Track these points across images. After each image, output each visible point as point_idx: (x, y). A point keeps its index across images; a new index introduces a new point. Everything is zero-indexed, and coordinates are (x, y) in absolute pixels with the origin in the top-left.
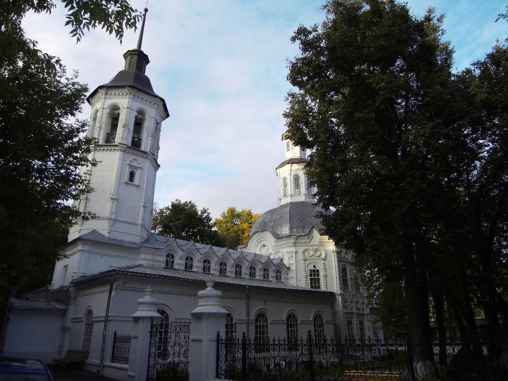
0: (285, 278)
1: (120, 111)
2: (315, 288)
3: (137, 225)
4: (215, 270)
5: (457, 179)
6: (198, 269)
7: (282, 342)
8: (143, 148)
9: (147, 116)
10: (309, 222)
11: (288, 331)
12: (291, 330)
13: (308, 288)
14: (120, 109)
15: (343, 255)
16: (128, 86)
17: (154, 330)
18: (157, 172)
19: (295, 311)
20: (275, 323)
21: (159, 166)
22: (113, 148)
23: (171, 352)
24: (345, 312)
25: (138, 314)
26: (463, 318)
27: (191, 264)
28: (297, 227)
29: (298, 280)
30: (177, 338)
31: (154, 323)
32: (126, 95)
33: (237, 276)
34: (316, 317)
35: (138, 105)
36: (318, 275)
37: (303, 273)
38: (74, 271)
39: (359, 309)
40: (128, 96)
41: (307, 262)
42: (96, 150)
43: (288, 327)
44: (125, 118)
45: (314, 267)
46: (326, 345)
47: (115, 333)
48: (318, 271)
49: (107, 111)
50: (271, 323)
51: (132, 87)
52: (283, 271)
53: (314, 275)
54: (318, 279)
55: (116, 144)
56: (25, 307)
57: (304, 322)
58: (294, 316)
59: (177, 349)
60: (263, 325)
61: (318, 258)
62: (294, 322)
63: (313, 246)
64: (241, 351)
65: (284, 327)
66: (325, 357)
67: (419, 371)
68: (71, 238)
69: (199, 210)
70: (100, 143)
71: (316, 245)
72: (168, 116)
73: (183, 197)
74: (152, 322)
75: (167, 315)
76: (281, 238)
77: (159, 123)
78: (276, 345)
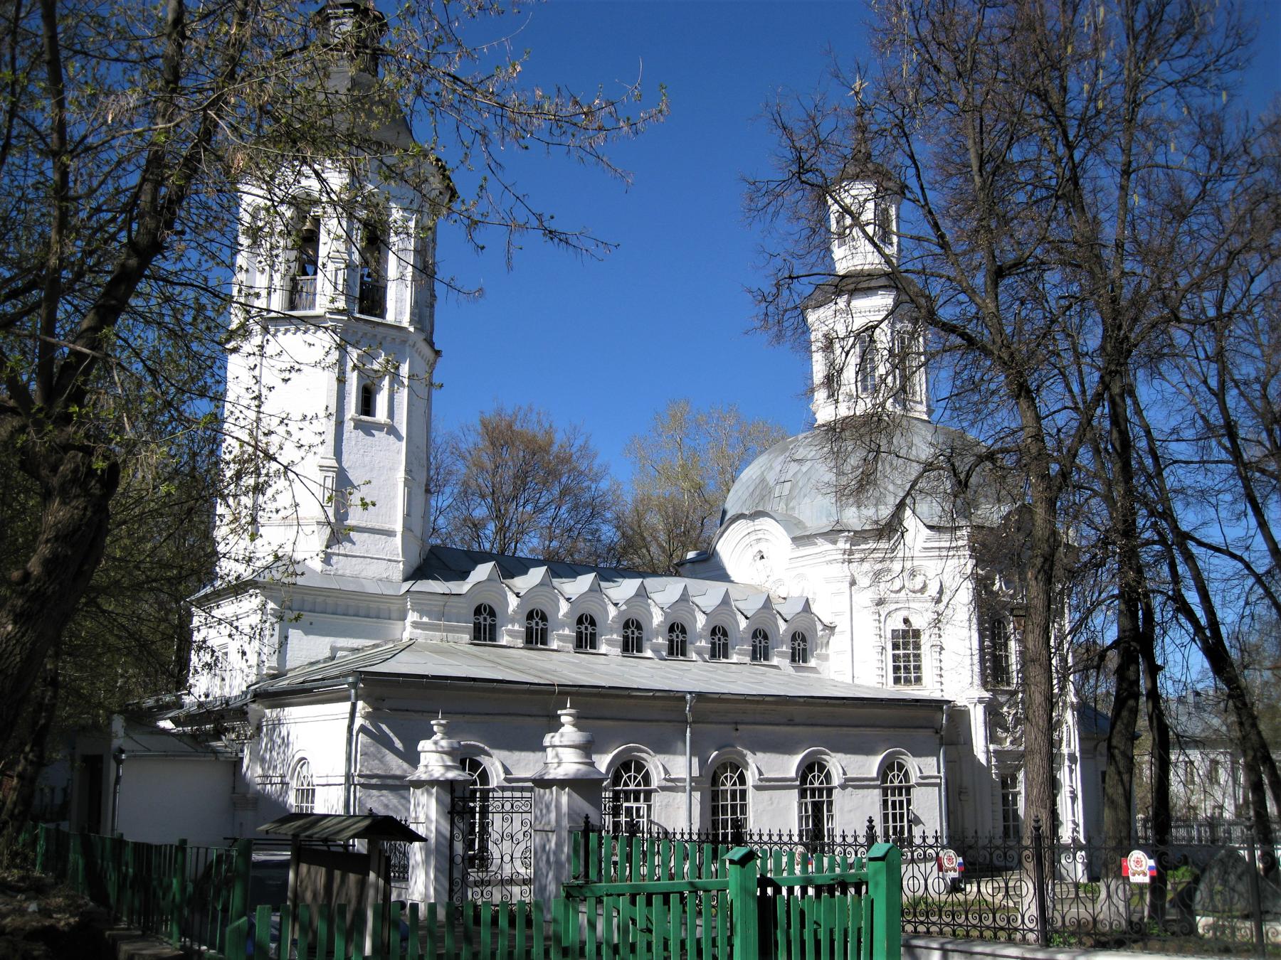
3: (390, 533)
7: (931, 841)
8: (390, 317)
11: (885, 802)
12: (894, 803)
13: (889, 689)
20: (767, 785)
23: (496, 855)
24: (995, 751)
29: (853, 666)
30: (505, 825)
36: (917, 646)
41: (884, 611)
45: (906, 621)
48: (917, 634)
50: (757, 788)
53: (907, 639)
55: (318, 311)
59: (507, 845)
61: (919, 595)
62: (822, 783)
65: (877, 793)
66: (922, 870)
67: (1031, 886)
76: (808, 537)
78: (850, 845)
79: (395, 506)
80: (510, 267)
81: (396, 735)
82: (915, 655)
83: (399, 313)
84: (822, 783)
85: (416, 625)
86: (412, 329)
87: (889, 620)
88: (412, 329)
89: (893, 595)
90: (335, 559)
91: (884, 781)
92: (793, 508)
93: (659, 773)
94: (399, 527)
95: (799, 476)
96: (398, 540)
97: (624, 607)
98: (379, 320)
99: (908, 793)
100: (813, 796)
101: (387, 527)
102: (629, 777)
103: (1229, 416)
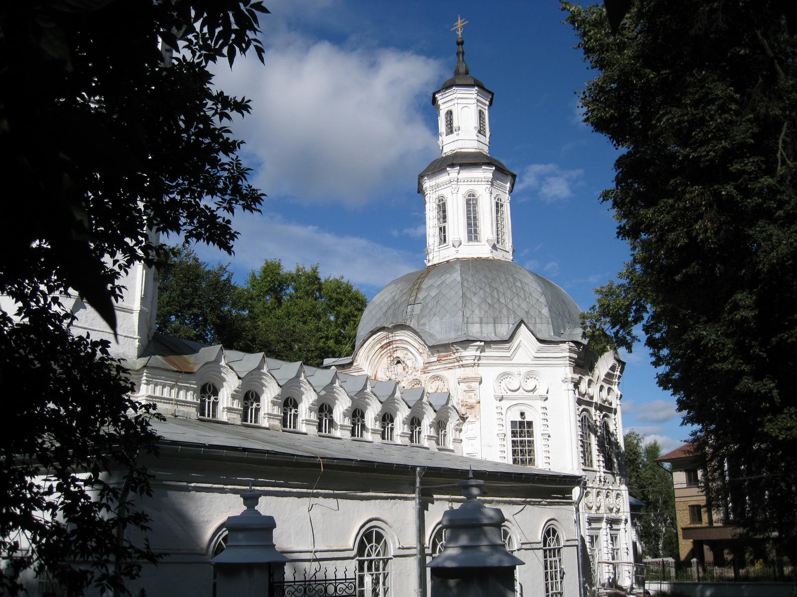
0: (455, 440)
2: (523, 462)
4: (308, 422)
5: (647, 148)
10: (508, 309)
11: (546, 561)
12: (551, 562)
15: (583, 387)
19: (556, 520)
27: (213, 402)
28: (481, 319)
33: (414, 444)
34: (368, 535)
36: (530, 434)
37: (496, 429)
39: (611, 510)
43: (545, 557)
45: (522, 414)
48: (530, 424)
52: (452, 422)
53: (522, 430)
54: (531, 443)
57: (524, 546)
58: (379, 537)
63: (518, 365)
71: (526, 365)
80: (263, 61)
81: (403, 493)
82: (529, 442)
87: (509, 412)
89: (510, 393)
91: (545, 545)
92: (424, 324)
93: (394, 543)
95: (428, 299)
96: (135, 317)
97: (323, 393)
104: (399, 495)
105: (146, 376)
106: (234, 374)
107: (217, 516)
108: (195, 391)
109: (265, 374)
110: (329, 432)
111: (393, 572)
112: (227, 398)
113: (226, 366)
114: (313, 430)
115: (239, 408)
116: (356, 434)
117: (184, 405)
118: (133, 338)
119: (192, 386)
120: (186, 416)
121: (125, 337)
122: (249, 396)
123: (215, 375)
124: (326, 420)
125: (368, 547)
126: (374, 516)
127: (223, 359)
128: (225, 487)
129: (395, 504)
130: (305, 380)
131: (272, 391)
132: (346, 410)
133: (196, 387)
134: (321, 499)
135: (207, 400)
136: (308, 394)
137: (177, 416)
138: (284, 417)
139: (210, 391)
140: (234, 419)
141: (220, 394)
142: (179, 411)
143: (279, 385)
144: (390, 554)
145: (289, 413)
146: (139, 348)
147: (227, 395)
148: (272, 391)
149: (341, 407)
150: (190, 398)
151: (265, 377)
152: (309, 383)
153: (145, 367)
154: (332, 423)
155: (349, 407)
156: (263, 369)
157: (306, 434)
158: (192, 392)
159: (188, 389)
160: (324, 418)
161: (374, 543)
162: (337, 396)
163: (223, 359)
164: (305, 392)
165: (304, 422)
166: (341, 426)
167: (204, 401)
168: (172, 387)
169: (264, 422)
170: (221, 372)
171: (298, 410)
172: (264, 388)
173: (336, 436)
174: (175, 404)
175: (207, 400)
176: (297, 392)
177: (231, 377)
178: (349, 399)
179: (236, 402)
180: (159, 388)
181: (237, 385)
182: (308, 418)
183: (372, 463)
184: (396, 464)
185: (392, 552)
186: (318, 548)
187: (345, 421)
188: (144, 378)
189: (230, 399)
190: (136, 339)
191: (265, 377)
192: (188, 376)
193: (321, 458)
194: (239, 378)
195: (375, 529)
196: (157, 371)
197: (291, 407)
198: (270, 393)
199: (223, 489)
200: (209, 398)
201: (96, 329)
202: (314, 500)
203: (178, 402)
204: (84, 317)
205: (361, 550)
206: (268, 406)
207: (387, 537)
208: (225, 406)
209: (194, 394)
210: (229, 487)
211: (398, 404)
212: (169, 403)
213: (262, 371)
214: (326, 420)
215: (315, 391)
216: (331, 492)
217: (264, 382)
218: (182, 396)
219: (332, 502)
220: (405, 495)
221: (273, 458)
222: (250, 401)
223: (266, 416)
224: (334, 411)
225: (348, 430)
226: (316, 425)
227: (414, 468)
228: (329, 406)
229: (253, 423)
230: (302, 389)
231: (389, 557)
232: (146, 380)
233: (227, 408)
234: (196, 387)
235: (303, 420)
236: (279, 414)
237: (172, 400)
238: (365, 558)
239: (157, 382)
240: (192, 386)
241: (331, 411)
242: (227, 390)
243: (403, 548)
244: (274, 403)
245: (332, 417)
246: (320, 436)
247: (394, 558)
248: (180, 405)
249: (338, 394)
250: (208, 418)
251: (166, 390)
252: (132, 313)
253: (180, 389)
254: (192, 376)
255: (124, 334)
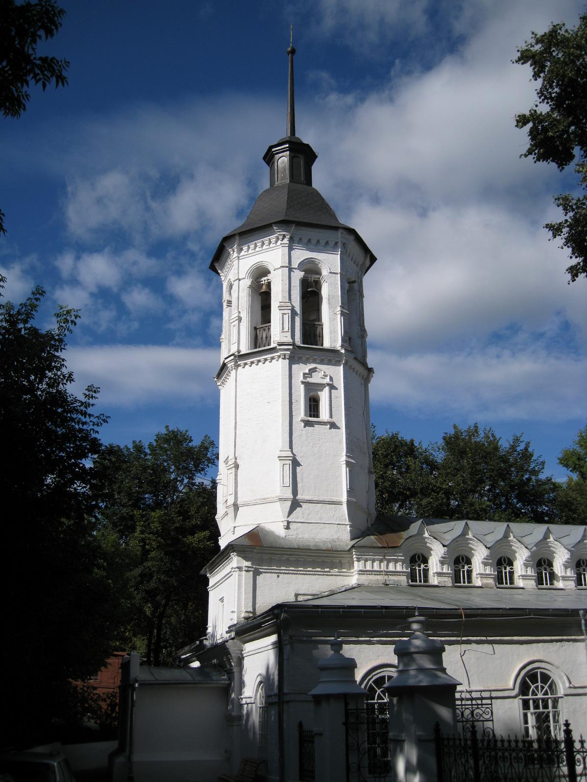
1: (270, 277)
3: (340, 503)
4: (524, 577)
6: (486, 581)
8: (327, 344)
9: (325, 272)
14: (269, 272)
16: (276, 223)
17: (352, 720)
18: (370, 385)
21: (370, 371)
22: (269, 356)
25: (319, 690)
26: (70, 679)
27: (424, 570)
31: (349, 707)
32: (276, 242)
35: (301, 255)
38: (233, 610)
40: (279, 242)
42: (239, 365)
44: (283, 292)
46: (532, 751)
47: (300, 725)
49: (248, 282)
51: (284, 223)
55: (273, 345)
56: (157, 680)
58: (545, 678)
60: (543, 700)
64: (471, 761)
68: (223, 543)
69: (504, 444)
70: (244, 351)
72: (373, 259)
73: (392, 430)
74: (346, 704)
75: (553, 681)
77: (354, 282)
79: (341, 482)
81: (570, 636)
83: (333, 340)
84: (546, 693)
85: (362, 572)
86: (343, 351)
88: (343, 351)
90: (292, 526)
93: (563, 683)
94: (344, 498)
96: (344, 507)
97: (535, 548)
98: (321, 347)
99: (555, 706)
100: (536, 707)
101: (335, 499)
102: (537, 687)
103: (237, 501)
104: (565, 638)
105: (355, 555)
106: (439, 543)
107: (366, 664)
108: (403, 562)
109: (471, 539)
110: (552, 584)
111: (565, 711)
112: (437, 565)
113: (430, 537)
114: (531, 584)
115: (450, 571)
116: (583, 583)
117: (395, 575)
118: (345, 525)
119: (399, 558)
120: (397, 583)
121: (338, 524)
122: (460, 561)
123: (505, 549)
124: (546, 574)
125: (533, 687)
126: (541, 658)
127: (426, 531)
128: (371, 639)
129: (562, 646)
130: (515, 540)
131: (480, 552)
132: (566, 562)
133: (403, 558)
134: (474, 646)
135: (417, 568)
136: (521, 551)
137: (388, 585)
138: (498, 575)
139: (584, 564)
140: (445, 581)
141: (430, 561)
142: (389, 580)
143: (486, 547)
144: (560, 692)
145: (504, 571)
146: (351, 531)
147: (436, 561)
148: (480, 552)
149: (560, 559)
150: (399, 568)
151: (471, 542)
152: (519, 541)
153: (353, 547)
154: (553, 576)
155: (568, 559)
156: (468, 535)
157: (523, 588)
158: (401, 563)
159: (396, 561)
160: (544, 572)
161: (539, 684)
162: (554, 550)
163: (426, 531)
164: (517, 550)
165: (521, 577)
166: (562, 577)
167: (502, 572)
168: (381, 561)
169: (434, 580)
170: (426, 543)
171: (514, 567)
172: (473, 551)
173: (558, 587)
174: (385, 575)
175: (417, 568)
176: (466, 548)
177: (436, 546)
178: (566, 551)
179: (445, 567)
180: (369, 563)
181: (443, 552)
182: (524, 573)
183: (566, 610)
184: (552, 609)
185: (561, 690)
186: (473, 688)
187: (568, 572)
188: (355, 556)
189: (439, 565)
190: (347, 525)
191: (471, 542)
192: (393, 550)
193: (463, 609)
194: (444, 546)
195: (539, 671)
196: (364, 549)
197: (505, 565)
198: (521, 557)
199: (370, 641)
200: (419, 566)
201: (312, 522)
202: (468, 646)
203: (388, 573)
204: (301, 514)
205: (524, 689)
206: (479, 567)
207: (554, 676)
208: (435, 571)
209: (403, 564)
210: (375, 639)
211: (554, 548)
212: (380, 575)
213: (467, 536)
214: (546, 574)
215: (526, 548)
216: (484, 638)
217: (472, 546)
218: (391, 567)
219: (487, 648)
220: (573, 637)
221: (504, 612)
222: (461, 565)
223: (479, 576)
224: (554, 564)
225: (572, 580)
226: (451, 577)
227: (577, 610)
228: (548, 560)
229: (466, 584)
230: (513, 548)
231: (559, 695)
232: (356, 558)
233: (436, 573)
234: (403, 558)
235: (519, 576)
236: (492, 573)
237: (382, 571)
238: (530, 697)
239: (367, 558)
240: (399, 558)
241: (550, 564)
242: (435, 558)
243: (575, 688)
244: (485, 564)
245: (552, 570)
246: (539, 589)
247: (565, 698)
248: (390, 575)
249: (554, 548)
250: (420, 584)
251: (376, 564)
252: (342, 505)
253: (389, 561)
254: (397, 549)
255: (337, 523)
